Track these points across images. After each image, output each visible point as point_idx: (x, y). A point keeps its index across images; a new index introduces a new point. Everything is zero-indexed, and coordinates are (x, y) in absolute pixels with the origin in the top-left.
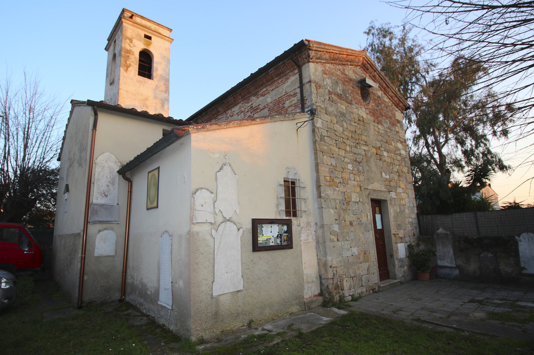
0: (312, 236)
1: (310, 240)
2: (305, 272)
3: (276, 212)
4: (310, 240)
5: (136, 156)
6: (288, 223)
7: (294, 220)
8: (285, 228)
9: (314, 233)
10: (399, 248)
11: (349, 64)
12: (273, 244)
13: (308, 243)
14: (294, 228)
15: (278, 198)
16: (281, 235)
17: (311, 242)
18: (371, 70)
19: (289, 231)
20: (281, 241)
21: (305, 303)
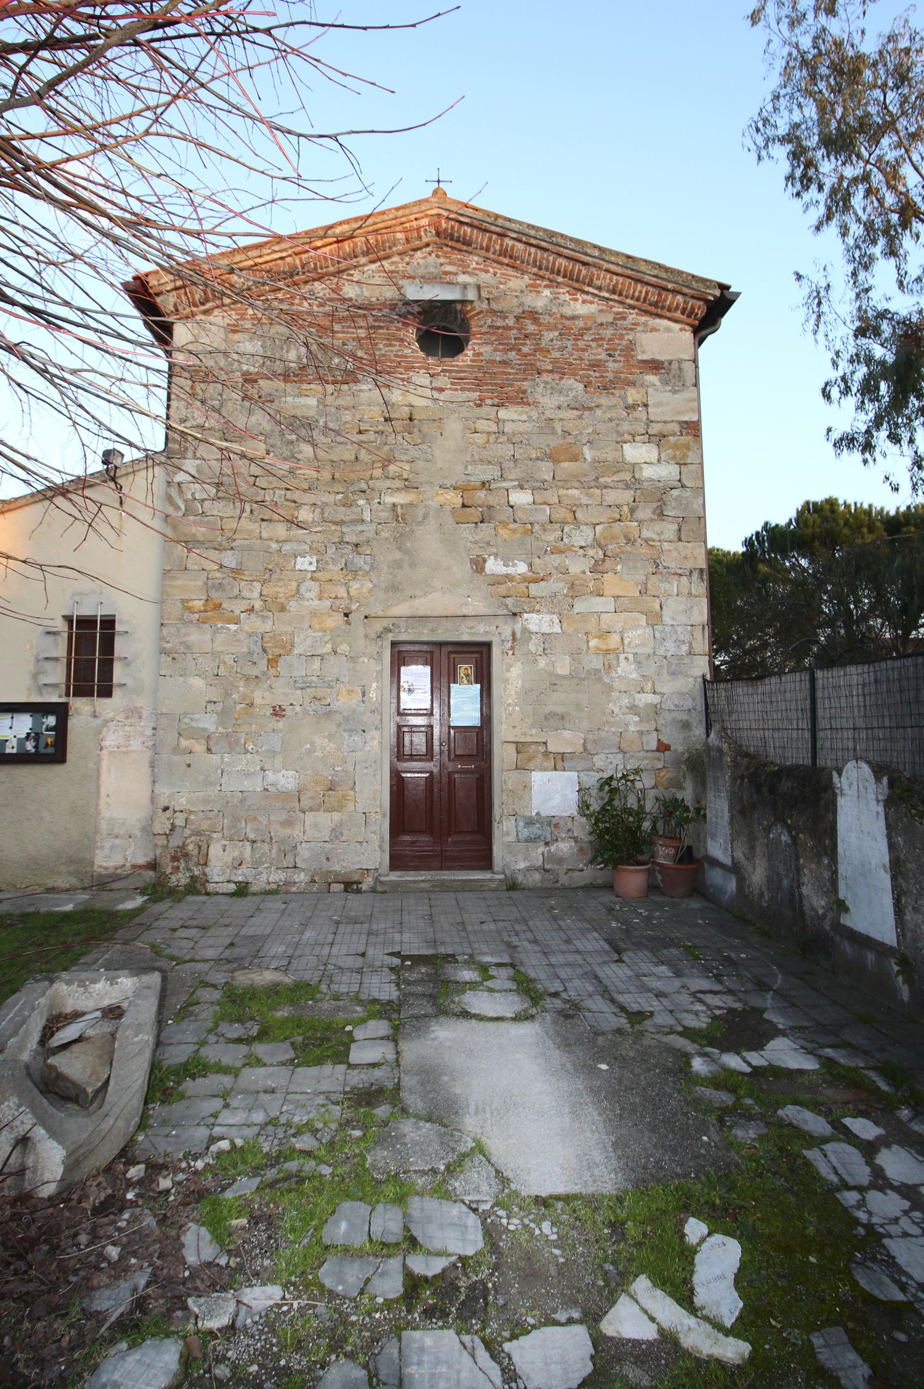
0: (141, 739)
1: (133, 748)
2: (106, 813)
3: (29, 689)
4: (135, 745)
5: (783, 514)
6: (61, 711)
7: (81, 707)
8: (51, 720)
9: (149, 732)
10: (535, 787)
11: (363, 260)
12: (15, 751)
13: (127, 753)
14: (74, 724)
15: (38, 660)
16: (37, 734)
17: (134, 751)
18: (481, 239)
19: (61, 729)
20: (36, 747)
21: (92, 876)
